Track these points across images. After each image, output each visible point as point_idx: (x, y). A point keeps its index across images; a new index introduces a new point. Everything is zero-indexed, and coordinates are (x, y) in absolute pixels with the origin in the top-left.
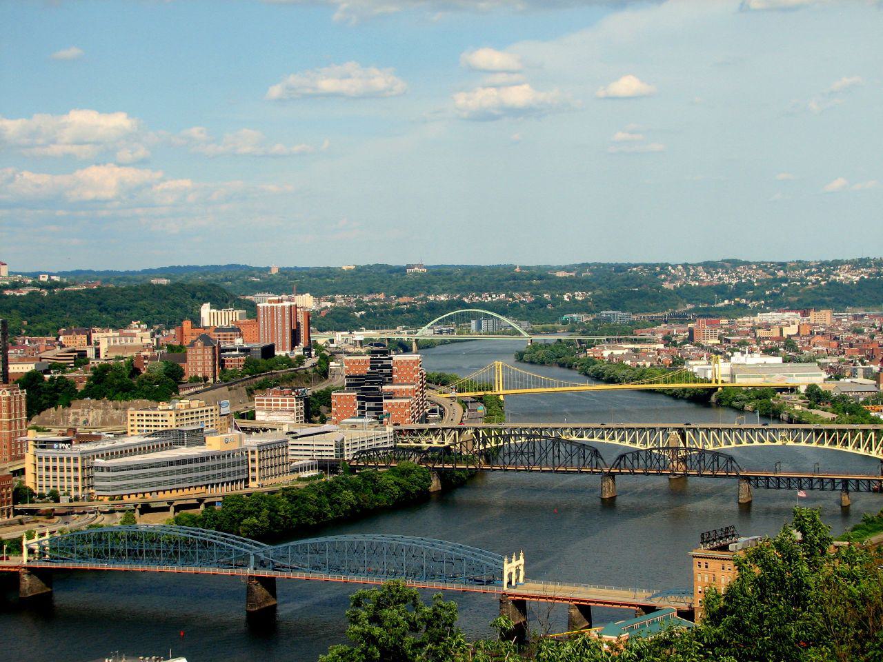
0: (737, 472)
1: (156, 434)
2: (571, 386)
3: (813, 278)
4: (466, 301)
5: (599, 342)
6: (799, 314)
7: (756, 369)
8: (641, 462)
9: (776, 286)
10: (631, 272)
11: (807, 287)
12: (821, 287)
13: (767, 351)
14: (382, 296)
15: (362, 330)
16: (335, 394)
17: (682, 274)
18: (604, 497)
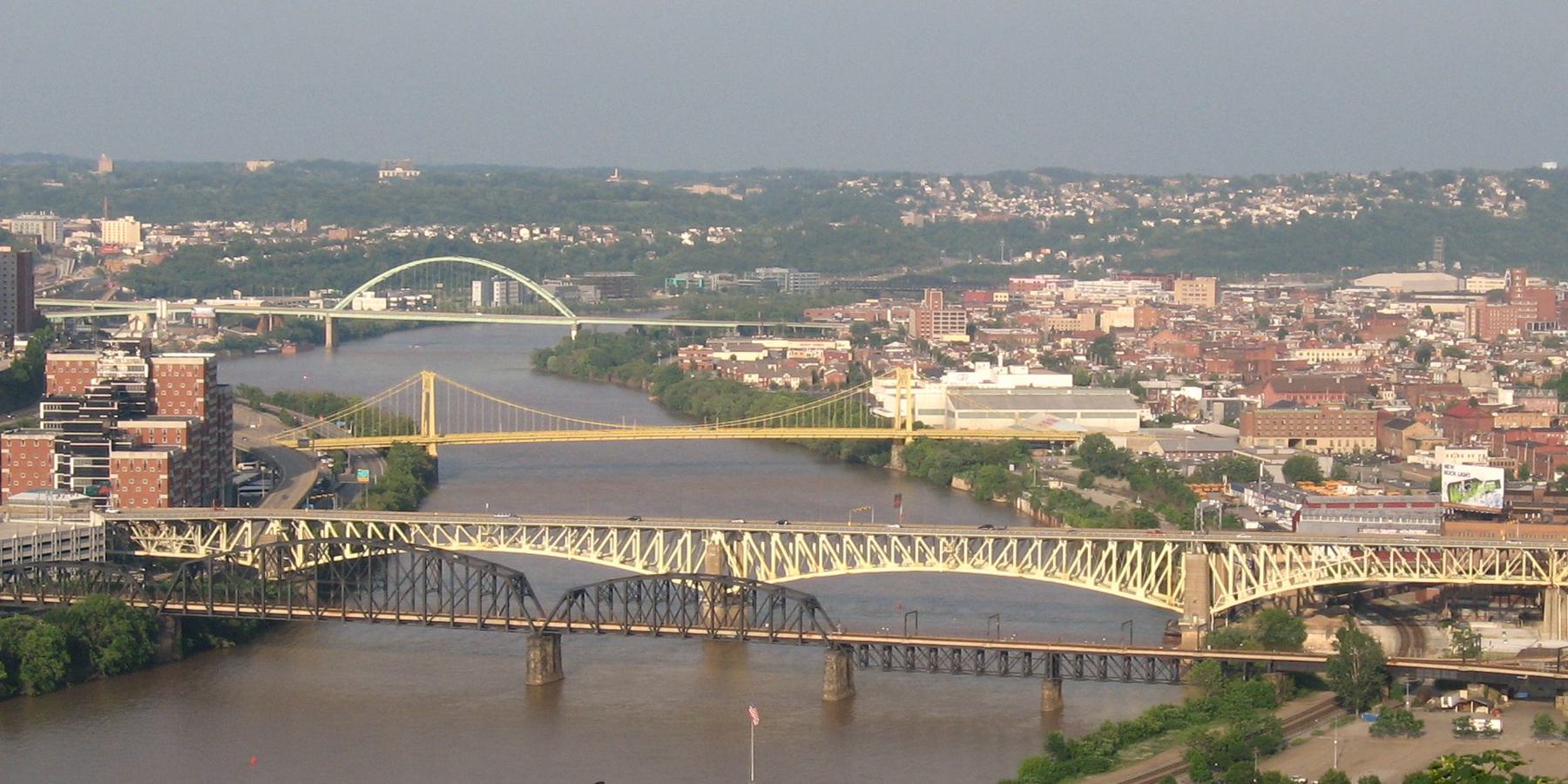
0: (825, 635)
1: (1551, 632)
2: (588, 428)
3: (1206, 211)
4: (476, 239)
5: (717, 332)
6: (1159, 284)
7: (1025, 398)
8: (618, 607)
9: (1132, 226)
10: (842, 189)
11: (1192, 230)
12: (1220, 230)
13: (1051, 363)
14: (302, 226)
16: (7, 437)
17: (948, 196)
18: (531, 682)
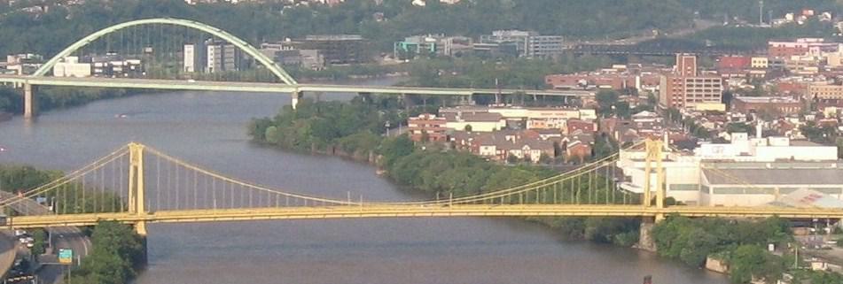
2: (311, 204)
15: (756, 218)
